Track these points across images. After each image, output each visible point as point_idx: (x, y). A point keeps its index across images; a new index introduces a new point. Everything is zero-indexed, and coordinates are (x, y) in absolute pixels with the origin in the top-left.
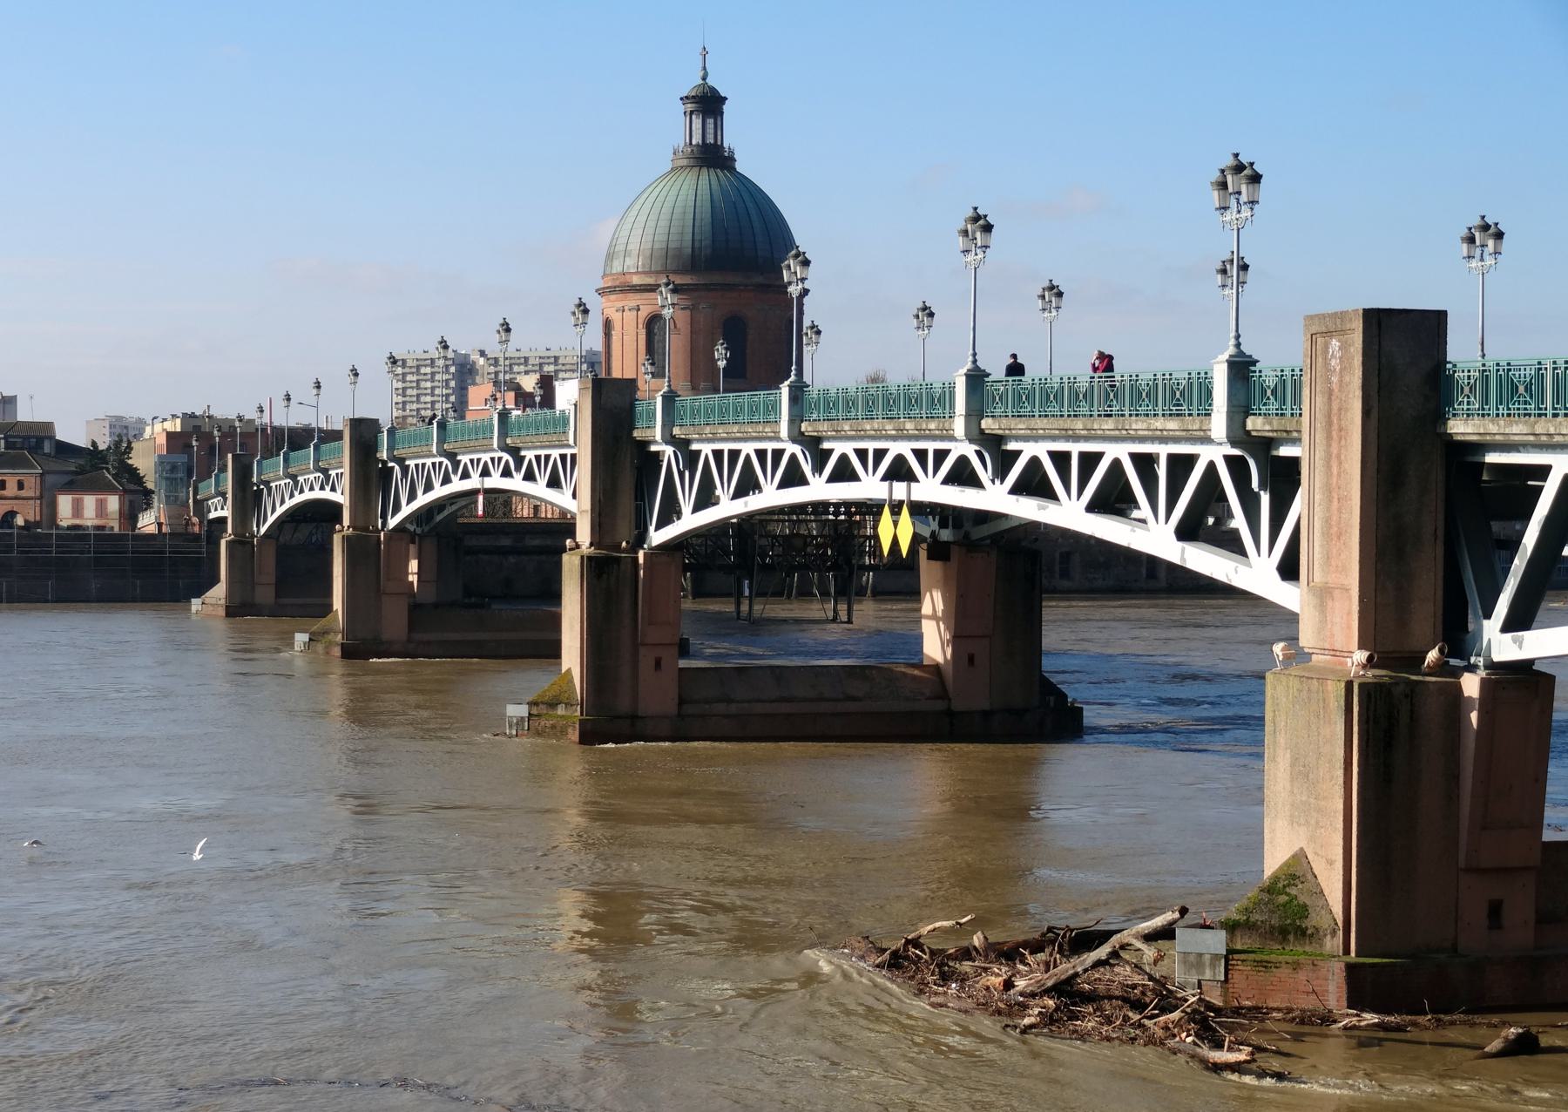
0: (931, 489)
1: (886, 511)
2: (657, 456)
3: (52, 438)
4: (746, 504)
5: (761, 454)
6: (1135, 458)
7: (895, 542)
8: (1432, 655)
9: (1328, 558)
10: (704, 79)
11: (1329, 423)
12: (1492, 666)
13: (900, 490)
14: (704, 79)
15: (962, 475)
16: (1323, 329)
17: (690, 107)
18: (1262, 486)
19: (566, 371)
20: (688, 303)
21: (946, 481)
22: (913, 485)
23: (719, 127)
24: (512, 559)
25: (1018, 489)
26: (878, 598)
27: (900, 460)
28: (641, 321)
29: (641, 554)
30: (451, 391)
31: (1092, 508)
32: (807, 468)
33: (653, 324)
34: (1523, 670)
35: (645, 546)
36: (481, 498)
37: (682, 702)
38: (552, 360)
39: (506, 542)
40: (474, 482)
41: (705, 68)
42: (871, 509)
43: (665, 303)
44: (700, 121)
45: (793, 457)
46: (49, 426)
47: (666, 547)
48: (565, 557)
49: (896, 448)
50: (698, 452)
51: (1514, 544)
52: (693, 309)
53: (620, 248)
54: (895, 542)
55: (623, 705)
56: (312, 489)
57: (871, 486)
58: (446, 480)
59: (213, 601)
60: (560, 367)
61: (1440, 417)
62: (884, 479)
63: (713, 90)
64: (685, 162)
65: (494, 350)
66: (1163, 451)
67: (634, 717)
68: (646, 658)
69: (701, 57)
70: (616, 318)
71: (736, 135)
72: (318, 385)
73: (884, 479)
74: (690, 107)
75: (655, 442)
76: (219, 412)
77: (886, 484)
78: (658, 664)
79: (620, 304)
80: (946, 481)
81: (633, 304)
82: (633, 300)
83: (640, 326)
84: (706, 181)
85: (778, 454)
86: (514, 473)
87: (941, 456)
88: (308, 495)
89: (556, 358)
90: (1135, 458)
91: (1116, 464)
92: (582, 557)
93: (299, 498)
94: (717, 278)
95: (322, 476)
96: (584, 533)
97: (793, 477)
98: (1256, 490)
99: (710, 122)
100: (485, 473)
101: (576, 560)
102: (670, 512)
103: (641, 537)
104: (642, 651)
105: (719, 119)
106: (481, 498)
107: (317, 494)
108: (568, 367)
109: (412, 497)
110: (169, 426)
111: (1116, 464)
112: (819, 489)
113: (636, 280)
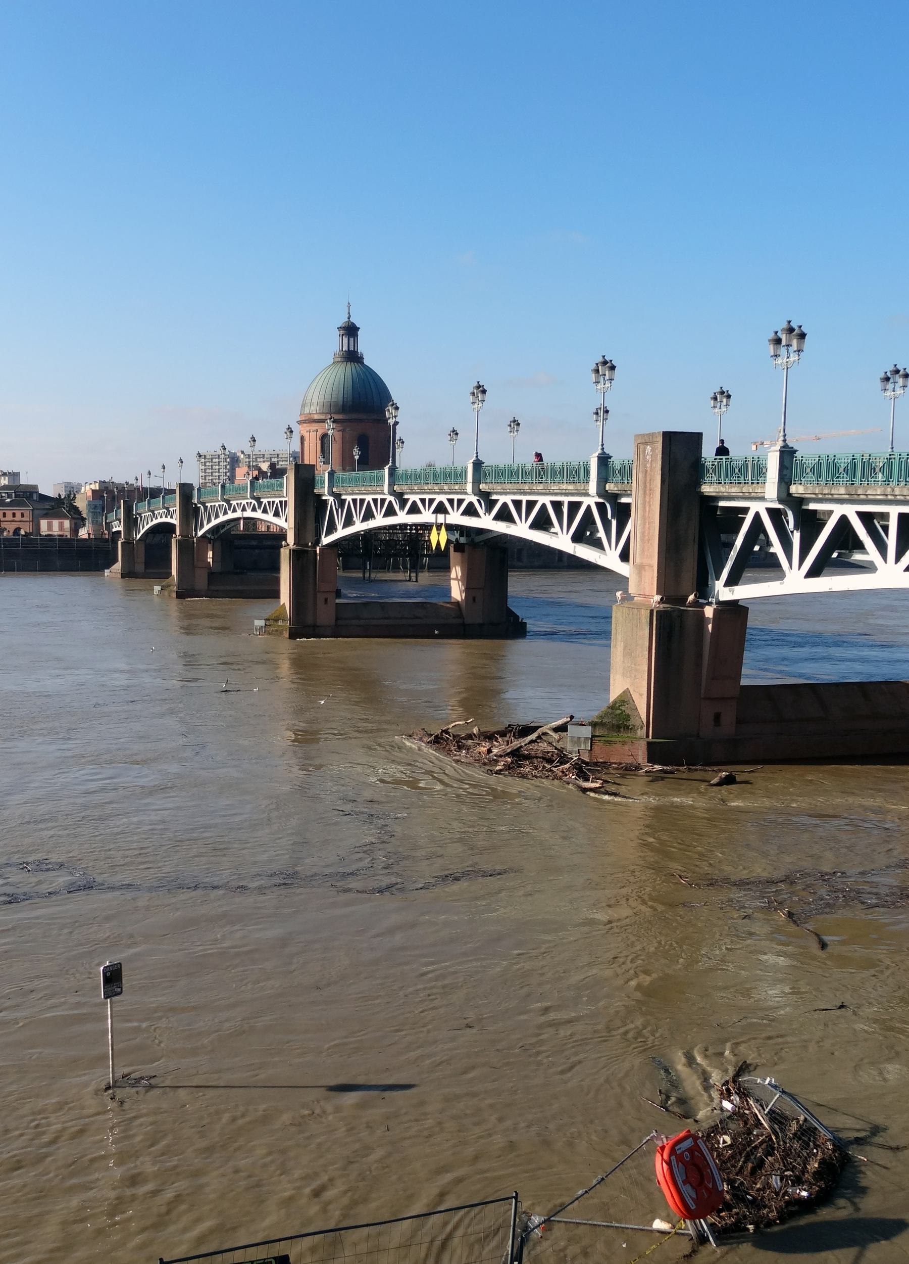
0: (456, 517)
1: (434, 528)
2: (326, 501)
3: (37, 492)
4: (368, 525)
5: (375, 501)
6: (553, 503)
7: (438, 544)
8: (691, 598)
9: (643, 551)
10: (349, 318)
11: (645, 487)
12: (719, 603)
13: (441, 518)
14: (349, 318)
15: (470, 511)
16: (643, 441)
17: (342, 332)
18: (613, 517)
19: (282, 461)
20: (341, 428)
21: (463, 514)
22: (447, 515)
23: (356, 342)
24: (257, 551)
25: (498, 518)
26: (431, 570)
27: (441, 504)
28: (318, 437)
29: (318, 549)
30: (227, 471)
31: (532, 527)
32: (397, 508)
33: (324, 437)
34: (733, 605)
35: (320, 545)
36: (242, 522)
37: (337, 619)
38: (276, 456)
39: (254, 543)
40: (238, 514)
41: (349, 313)
42: (427, 527)
43: (329, 428)
44: (347, 339)
45: (390, 502)
46: (36, 487)
47: (329, 545)
48: (282, 550)
49: (439, 498)
50: (345, 500)
51: (731, 545)
52: (343, 431)
53: (308, 401)
54: (438, 544)
55: (310, 620)
56: (161, 517)
57: (426, 516)
58: (225, 513)
59: (115, 571)
60: (279, 459)
61: (699, 485)
62: (433, 513)
63: (353, 324)
64: (339, 359)
65: (248, 451)
66: (566, 500)
67: (315, 626)
68: (320, 598)
69: (348, 308)
70: (306, 435)
71: (364, 346)
72: (164, 467)
73: (433, 513)
74: (342, 332)
75: (325, 495)
76: (117, 480)
77: (435, 515)
78: (326, 600)
79: (308, 429)
80: (463, 514)
81: (315, 429)
82: (315, 426)
83: (318, 439)
84: (350, 368)
85: (383, 501)
86: (258, 510)
87: (460, 502)
88: (159, 520)
89: (278, 455)
90: (553, 503)
91: (544, 506)
92: (290, 550)
93: (155, 522)
94: (354, 416)
95: (225, 504)
96: (291, 539)
97: (390, 512)
98: (610, 519)
99: (352, 339)
100: (244, 510)
101: (287, 552)
102: (332, 528)
103: (318, 541)
104: (319, 595)
105: (356, 338)
106: (242, 522)
107: (164, 520)
108: (283, 459)
109: (209, 521)
110: (93, 487)
111: (544, 506)
112: (402, 517)
113: (316, 417)
